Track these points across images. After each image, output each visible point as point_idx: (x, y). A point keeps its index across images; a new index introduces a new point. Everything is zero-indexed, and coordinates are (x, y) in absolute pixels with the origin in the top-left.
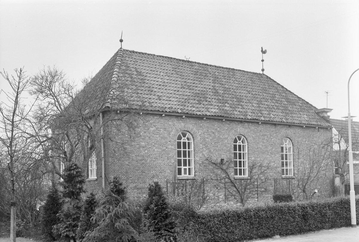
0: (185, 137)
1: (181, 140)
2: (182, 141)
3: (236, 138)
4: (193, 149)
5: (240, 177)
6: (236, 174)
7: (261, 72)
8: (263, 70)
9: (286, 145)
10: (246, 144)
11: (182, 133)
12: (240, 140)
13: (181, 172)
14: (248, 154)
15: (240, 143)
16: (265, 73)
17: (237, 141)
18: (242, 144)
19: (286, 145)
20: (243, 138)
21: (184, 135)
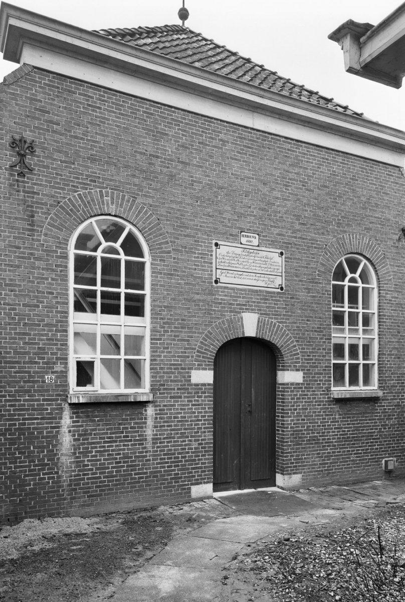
0: (355, 273)
1: (343, 281)
2: (346, 283)
3: (340, 265)
4: (375, 311)
5: (127, 395)
6: (339, 379)
7: (179, 22)
8: (184, 14)
9: (353, 280)
10: (374, 284)
11: (347, 260)
12: (353, 271)
13: (358, 378)
14: (379, 315)
15: (356, 282)
16: (189, 24)
17: (345, 275)
18: (360, 284)
19: (353, 280)
20: (365, 263)
21: (353, 265)
